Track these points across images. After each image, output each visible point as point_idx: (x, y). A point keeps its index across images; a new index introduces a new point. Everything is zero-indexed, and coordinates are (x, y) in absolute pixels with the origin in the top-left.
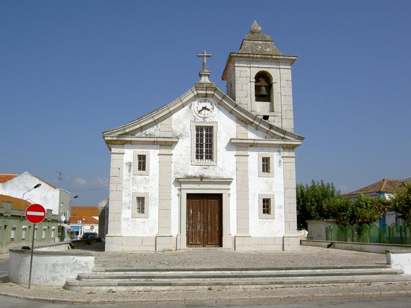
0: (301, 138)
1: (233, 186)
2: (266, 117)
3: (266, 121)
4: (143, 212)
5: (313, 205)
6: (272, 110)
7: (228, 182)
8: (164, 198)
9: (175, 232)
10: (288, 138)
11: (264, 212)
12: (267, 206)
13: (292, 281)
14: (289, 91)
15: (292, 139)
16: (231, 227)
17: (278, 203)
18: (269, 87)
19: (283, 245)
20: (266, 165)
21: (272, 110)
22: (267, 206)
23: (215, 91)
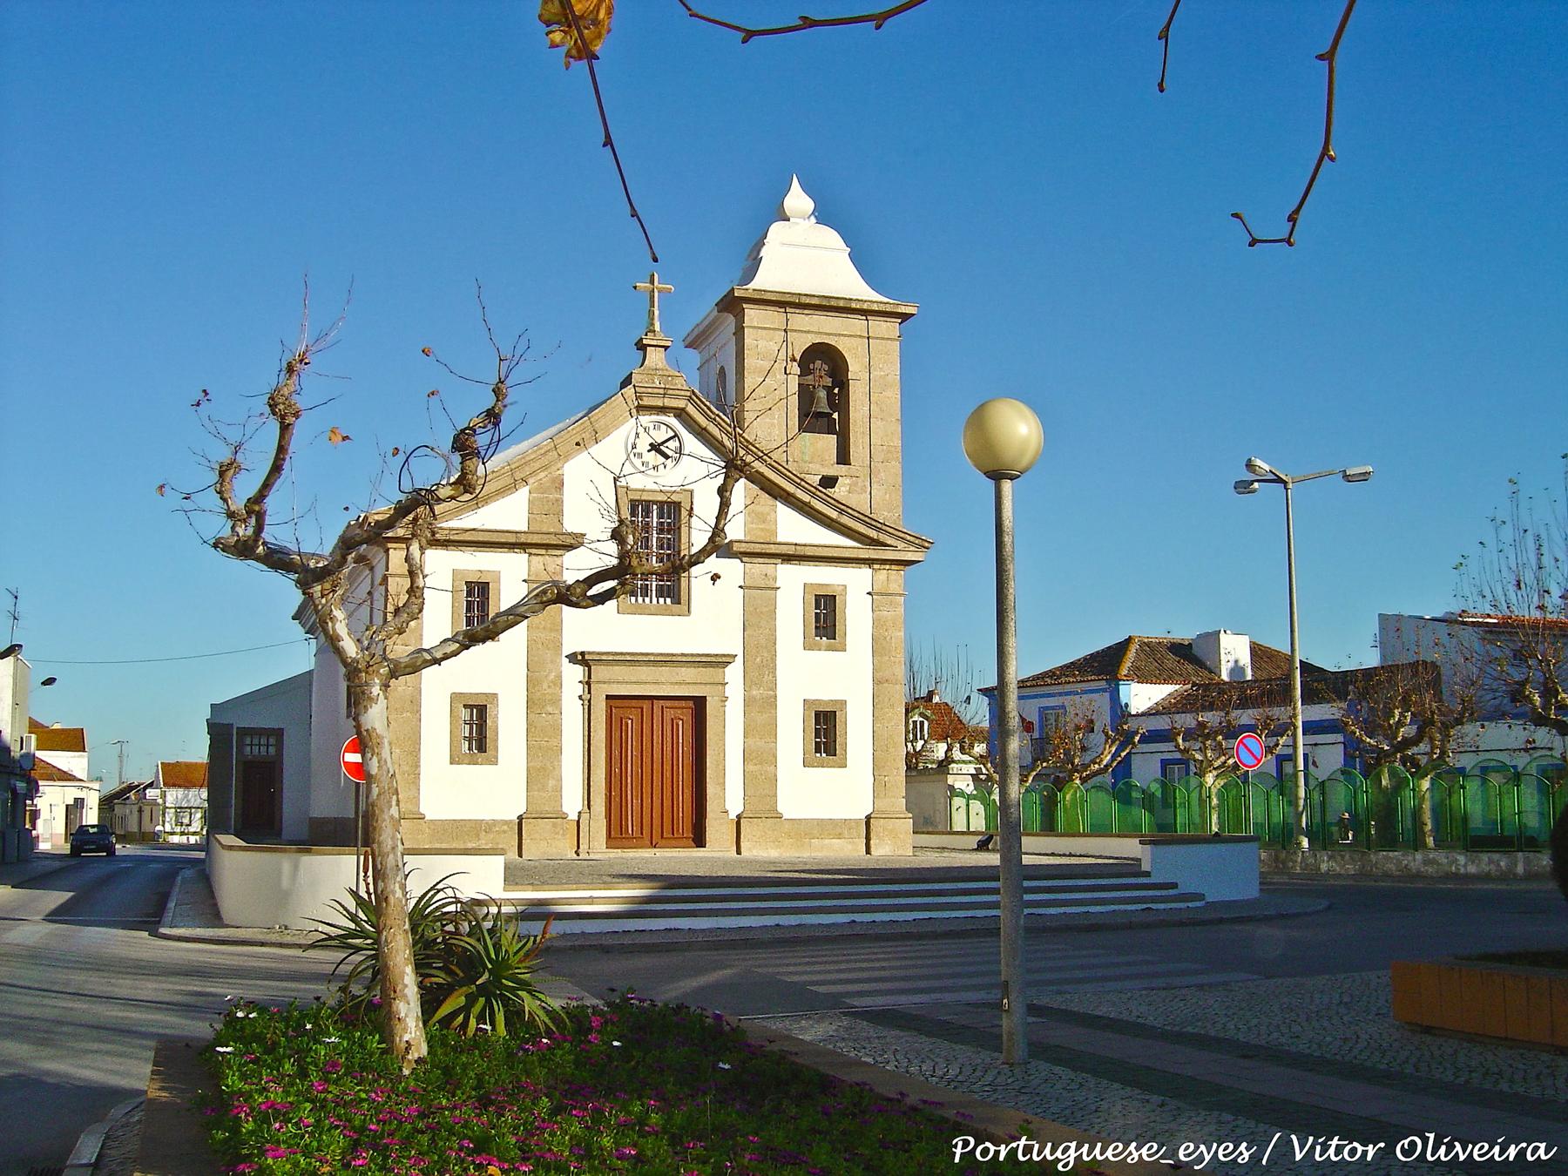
0: (923, 545)
1: (734, 674)
2: (828, 482)
3: (830, 491)
4: (482, 748)
5: (642, 1122)
6: (843, 457)
7: (720, 662)
8: (541, 702)
9: (572, 803)
10: (889, 541)
11: (818, 750)
12: (825, 730)
13: (37, 1012)
14: (892, 397)
15: (901, 545)
16: (729, 793)
17: (858, 733)
18: (840, 400)
19: (868, 838)
20: (825, 618)
21: (843, 457)
22: (825, 730)
23: (690, 399)
